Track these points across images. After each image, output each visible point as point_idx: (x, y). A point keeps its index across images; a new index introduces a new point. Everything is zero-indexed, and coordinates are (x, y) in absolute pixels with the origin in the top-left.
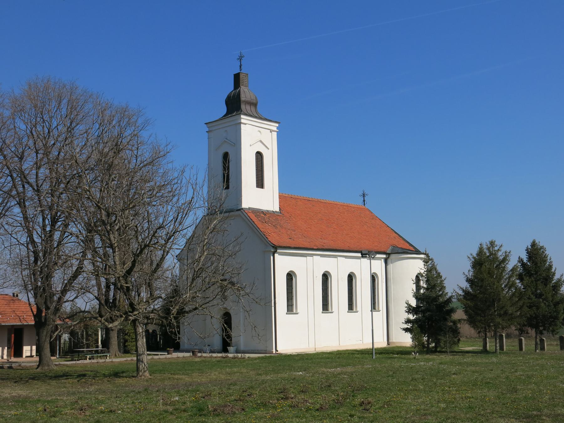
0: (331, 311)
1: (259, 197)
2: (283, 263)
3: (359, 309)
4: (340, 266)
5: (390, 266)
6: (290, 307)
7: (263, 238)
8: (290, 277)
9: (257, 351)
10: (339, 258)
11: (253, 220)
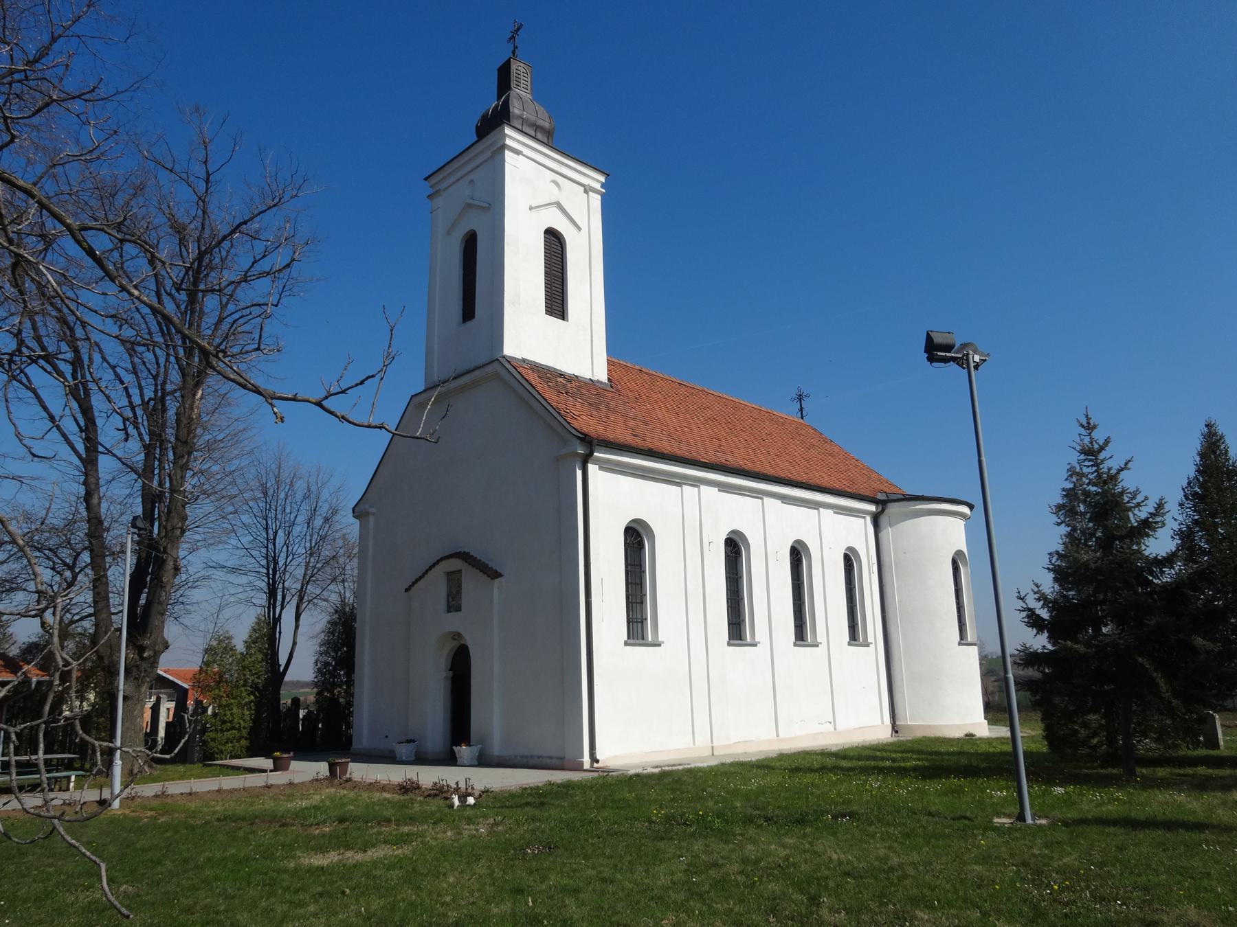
0: (756, 638)
1: (559, 337)
2: (613, 497)
3: (821, 637)
4: (775, 522)
5: (888, 533)
6: (638, 625)
7: (559, 431)
8: (636, 538)
9: (536, 761)
10: (766, 499)
11: (532, 389)
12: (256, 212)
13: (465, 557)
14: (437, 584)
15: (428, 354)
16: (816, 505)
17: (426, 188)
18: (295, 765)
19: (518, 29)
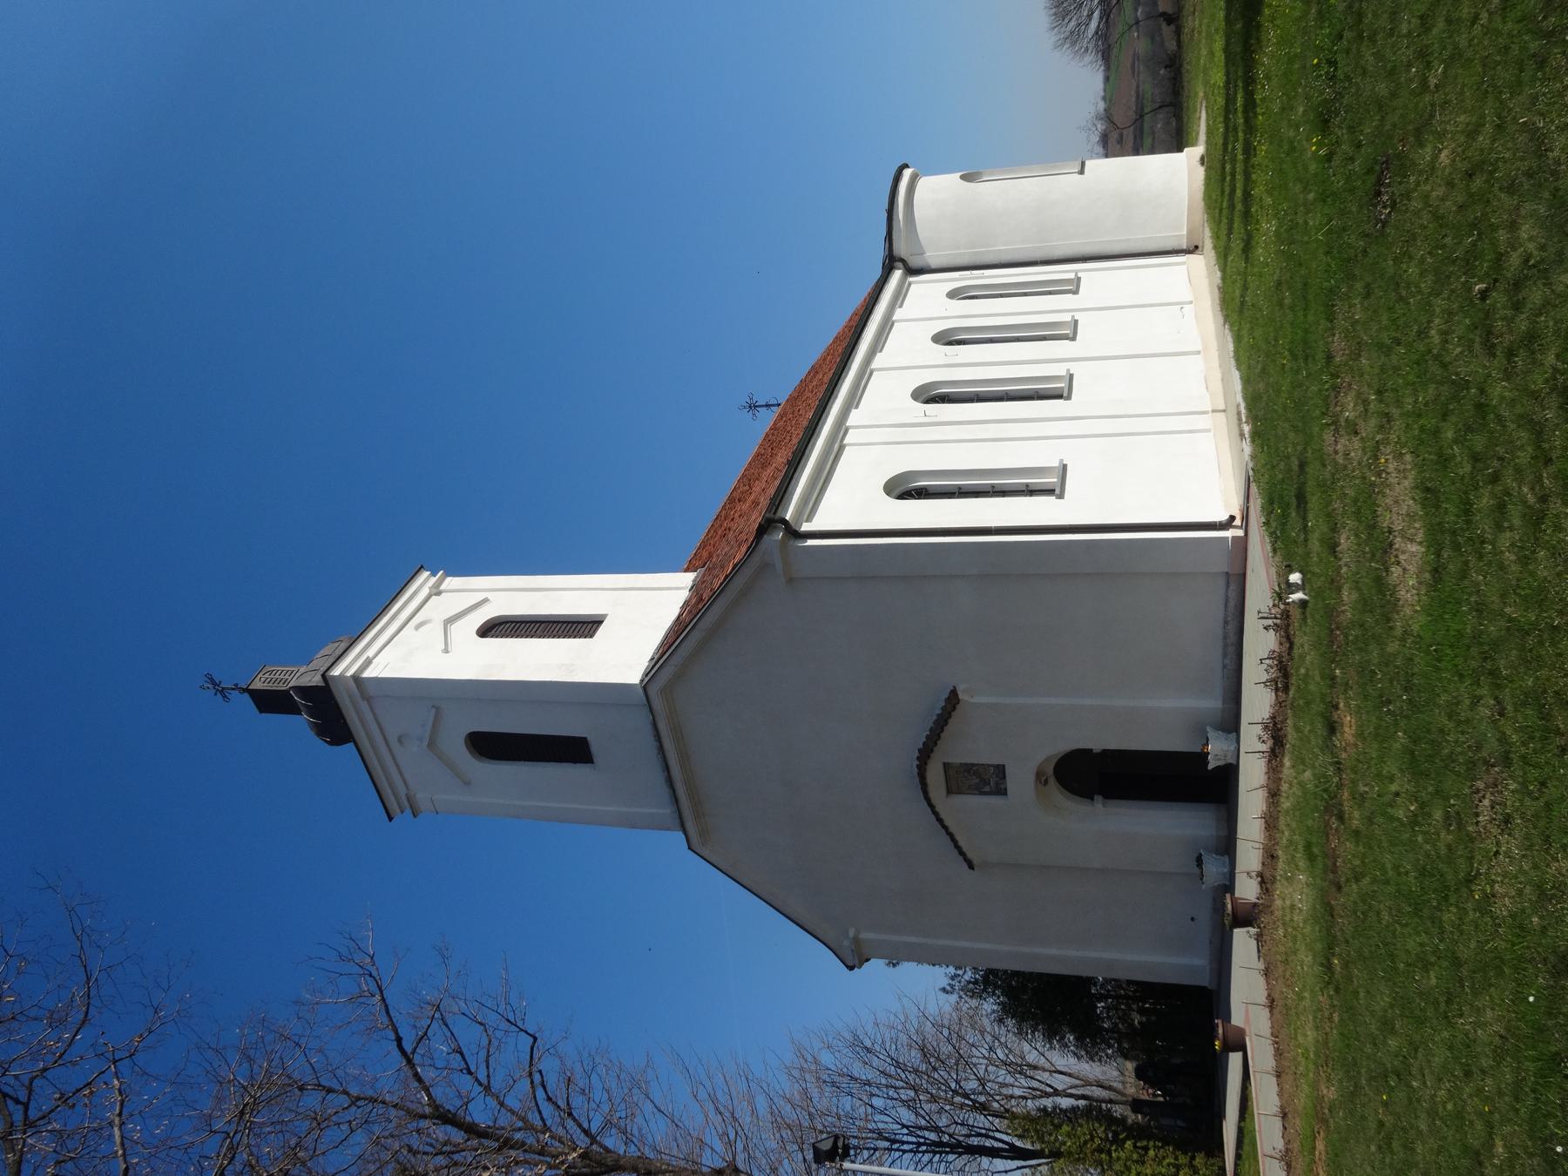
1: (629, 620)
5: (932, 257)
8: (905, 488)
9: (1231, 628)
10: (874, 365)
12: (386, 1020)
13: (925, 754)
14: (965, 810)
15: (633, 825)
16: (887, 325)
17: (403, 819)
18: (1237, 1019)
19: (212, 681)
